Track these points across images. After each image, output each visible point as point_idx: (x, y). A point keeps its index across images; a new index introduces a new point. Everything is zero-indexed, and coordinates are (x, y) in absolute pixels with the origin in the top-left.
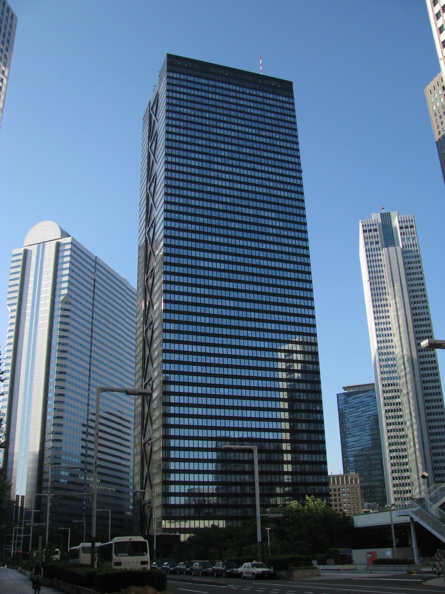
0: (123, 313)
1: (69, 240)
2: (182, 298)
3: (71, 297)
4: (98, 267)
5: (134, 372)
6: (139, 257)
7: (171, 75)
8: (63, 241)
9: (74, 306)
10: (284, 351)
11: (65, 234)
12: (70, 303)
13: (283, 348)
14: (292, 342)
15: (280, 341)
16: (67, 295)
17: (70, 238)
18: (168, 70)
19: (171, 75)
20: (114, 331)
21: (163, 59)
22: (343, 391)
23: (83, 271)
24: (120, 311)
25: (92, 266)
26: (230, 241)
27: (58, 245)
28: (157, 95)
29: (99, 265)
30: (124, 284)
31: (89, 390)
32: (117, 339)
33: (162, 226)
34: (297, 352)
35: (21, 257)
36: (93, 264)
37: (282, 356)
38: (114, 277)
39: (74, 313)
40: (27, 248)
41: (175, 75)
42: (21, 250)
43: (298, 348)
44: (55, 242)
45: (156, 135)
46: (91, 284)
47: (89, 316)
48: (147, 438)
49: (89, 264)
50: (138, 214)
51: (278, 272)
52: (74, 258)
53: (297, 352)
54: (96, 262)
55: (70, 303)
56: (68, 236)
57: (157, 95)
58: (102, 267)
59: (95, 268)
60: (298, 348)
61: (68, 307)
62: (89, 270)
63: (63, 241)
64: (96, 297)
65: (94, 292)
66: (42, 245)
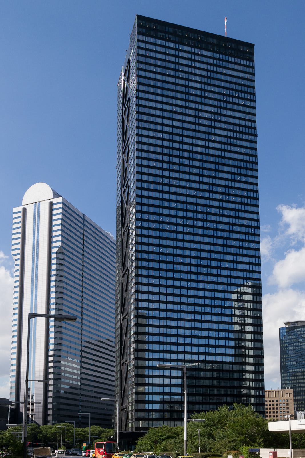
0: (108, 252)
1: (60, 199)
2: (193, 71)
3: (65, 249)
4: (86, 223)
5: (114, 335)
6: (117, 221)
7: (140, 38)
8: (55, 201)
9: (67, 256)
10: (237, 293)
11: (56, 195)
12: (63, 253)
13: (236, 290)
14: (244, 286)
15: (234, 285)
16: (61, 247)
17: (61, 198)
18: (139, 33)
19: (140, 38)
20: (99, 320)
21: (133, 22)
22: (284, 326)
23: (74, 225)
24: (106, 270)
25: (81, 228)
26: (174, 267)
27: (51, 204)
28: (129, 62)
29: (87, 221)
30: (108, 238)
31: (82, 331)
32: (98, 331)
33: (134, 195)
34: (247, 294)
35: (21, 214)
36: (82, 221)
37: (235, 296)
38: (100, 232)
39: (67, 278)
40: (25, 206)
41: (145, 39)
42: (20, 209)
43: (249, 290)
44: (49, 201)
45: (129, 102)
46: (80, 238)
47: (79, 290)
48: (124, 405)
49: (78, 252)
50: (116, 176)
51: (172, 380)
52: (64, 243)
53: (247, 294)
54: (84, 219)
55: (63, 253)
56: (60, 196)
57: (129, 62)
58: (89, 223)
59: (83, 224)
60: (249, 290)
61: (61, 256)
62: (78, 231)
63: (55, 201)
64: (85, 243)
65: (83, 244)
66: (37, 205)
